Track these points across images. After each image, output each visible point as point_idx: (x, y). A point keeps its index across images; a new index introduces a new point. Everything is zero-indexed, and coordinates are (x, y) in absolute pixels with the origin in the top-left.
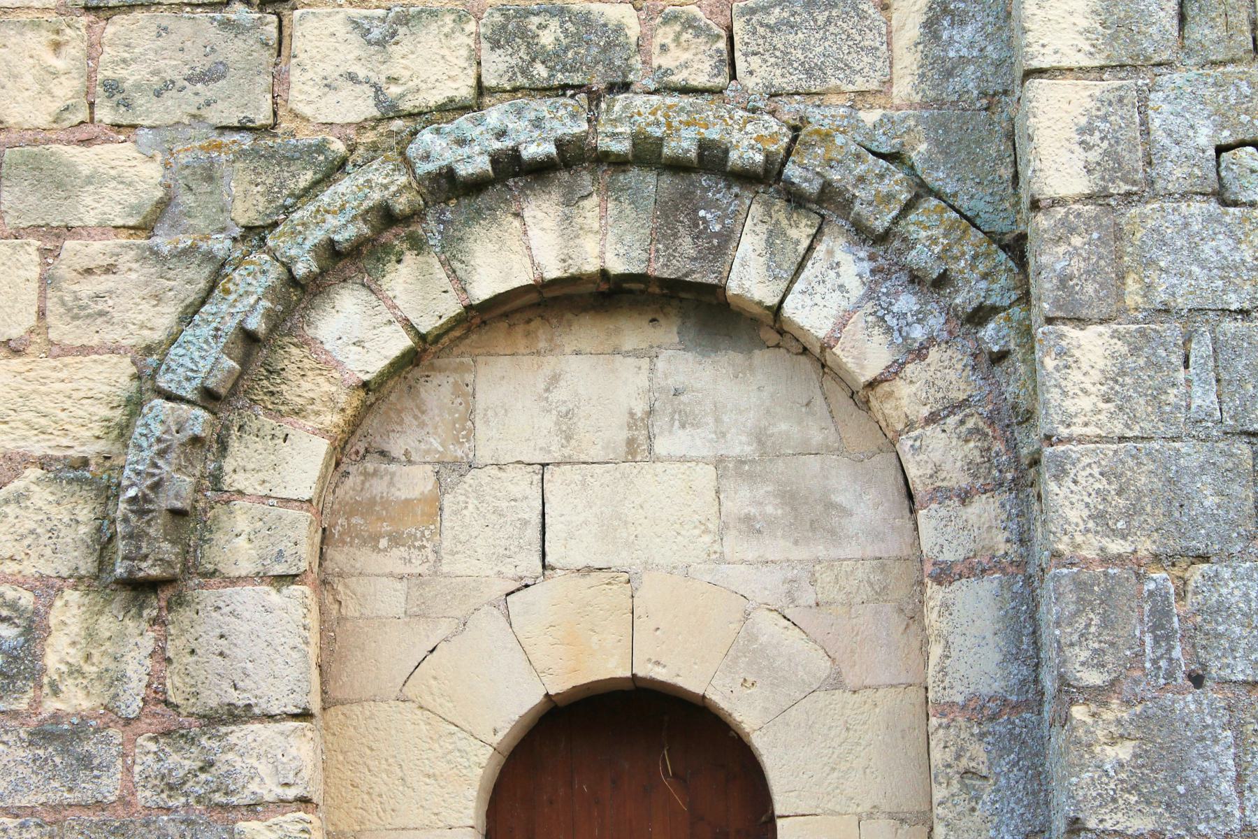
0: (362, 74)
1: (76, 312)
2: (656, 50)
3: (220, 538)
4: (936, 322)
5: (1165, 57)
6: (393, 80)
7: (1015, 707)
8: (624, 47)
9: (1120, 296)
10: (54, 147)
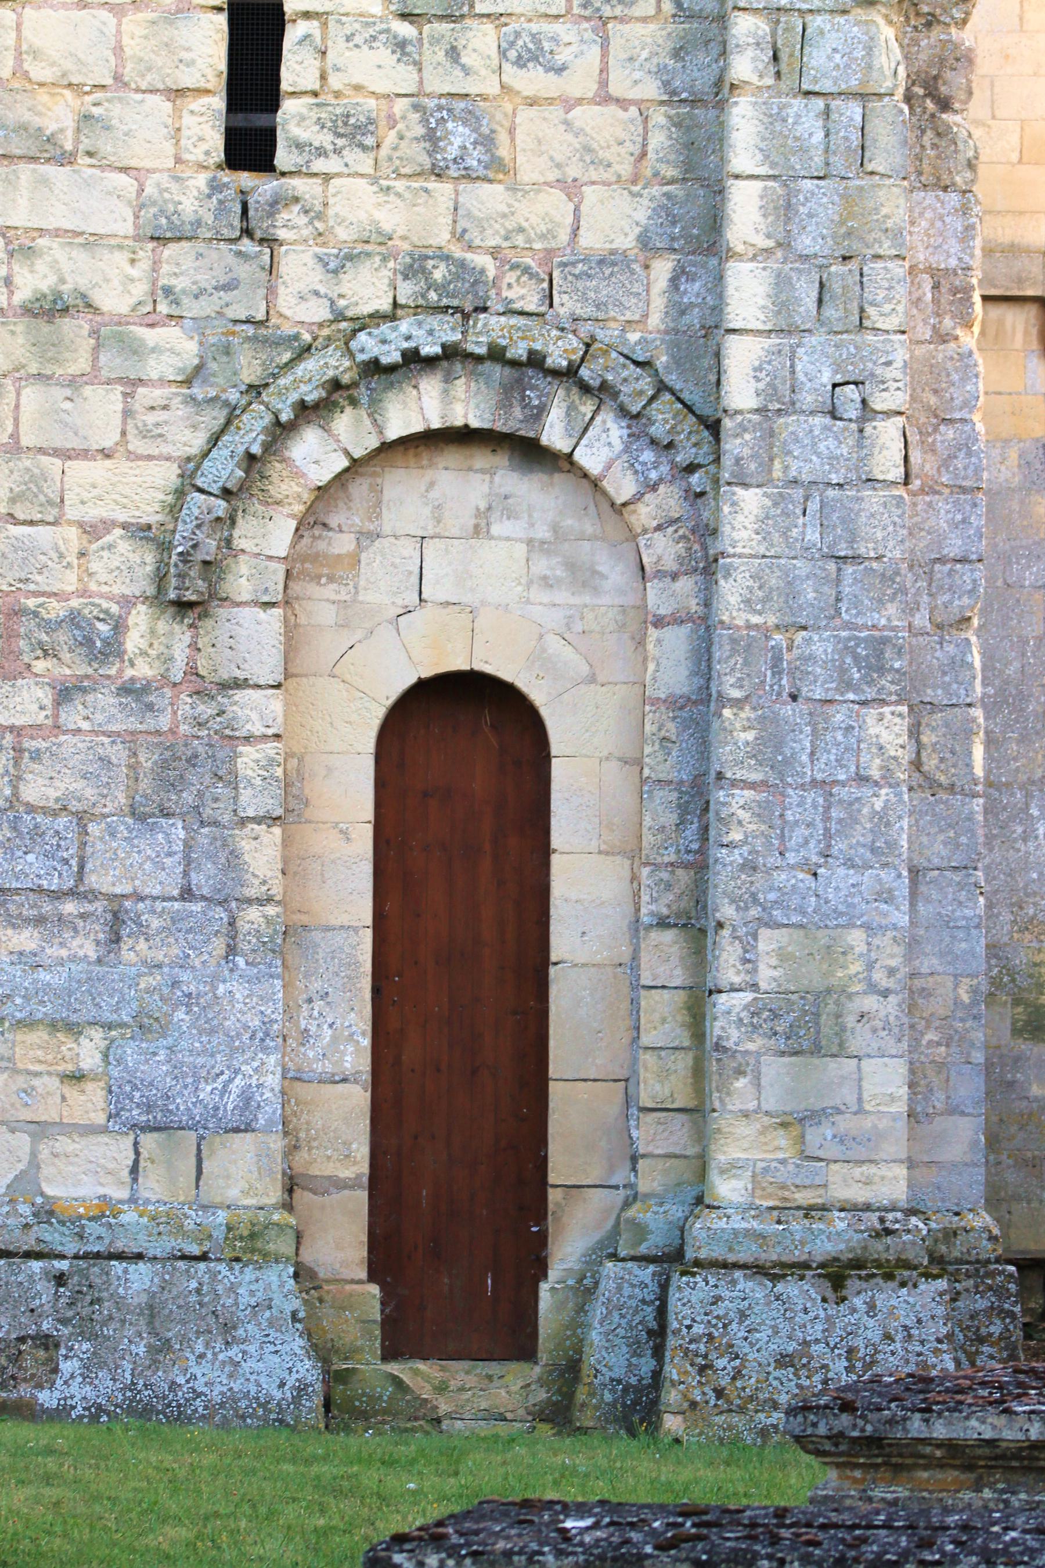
0: (322, 291)
1: (145, 434)
2: (504, 286)
3: (230, 577)
4: (665, 469)
5: (807, 327)
6: (341, 296)
7: (695, 702)
8: (486, 283)
9: (770, 471)
10: (132, 328)
